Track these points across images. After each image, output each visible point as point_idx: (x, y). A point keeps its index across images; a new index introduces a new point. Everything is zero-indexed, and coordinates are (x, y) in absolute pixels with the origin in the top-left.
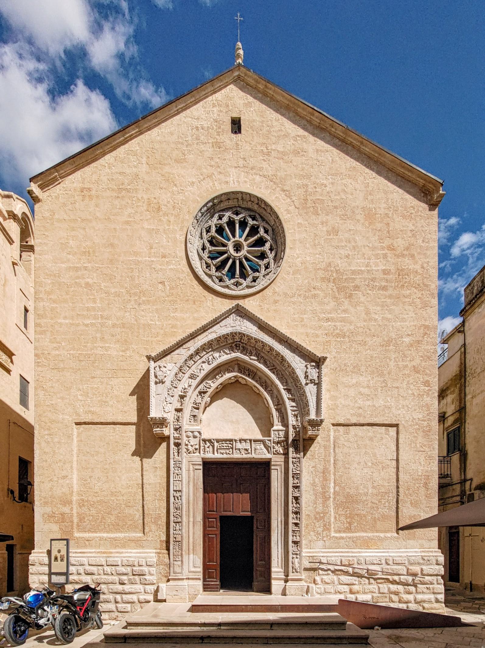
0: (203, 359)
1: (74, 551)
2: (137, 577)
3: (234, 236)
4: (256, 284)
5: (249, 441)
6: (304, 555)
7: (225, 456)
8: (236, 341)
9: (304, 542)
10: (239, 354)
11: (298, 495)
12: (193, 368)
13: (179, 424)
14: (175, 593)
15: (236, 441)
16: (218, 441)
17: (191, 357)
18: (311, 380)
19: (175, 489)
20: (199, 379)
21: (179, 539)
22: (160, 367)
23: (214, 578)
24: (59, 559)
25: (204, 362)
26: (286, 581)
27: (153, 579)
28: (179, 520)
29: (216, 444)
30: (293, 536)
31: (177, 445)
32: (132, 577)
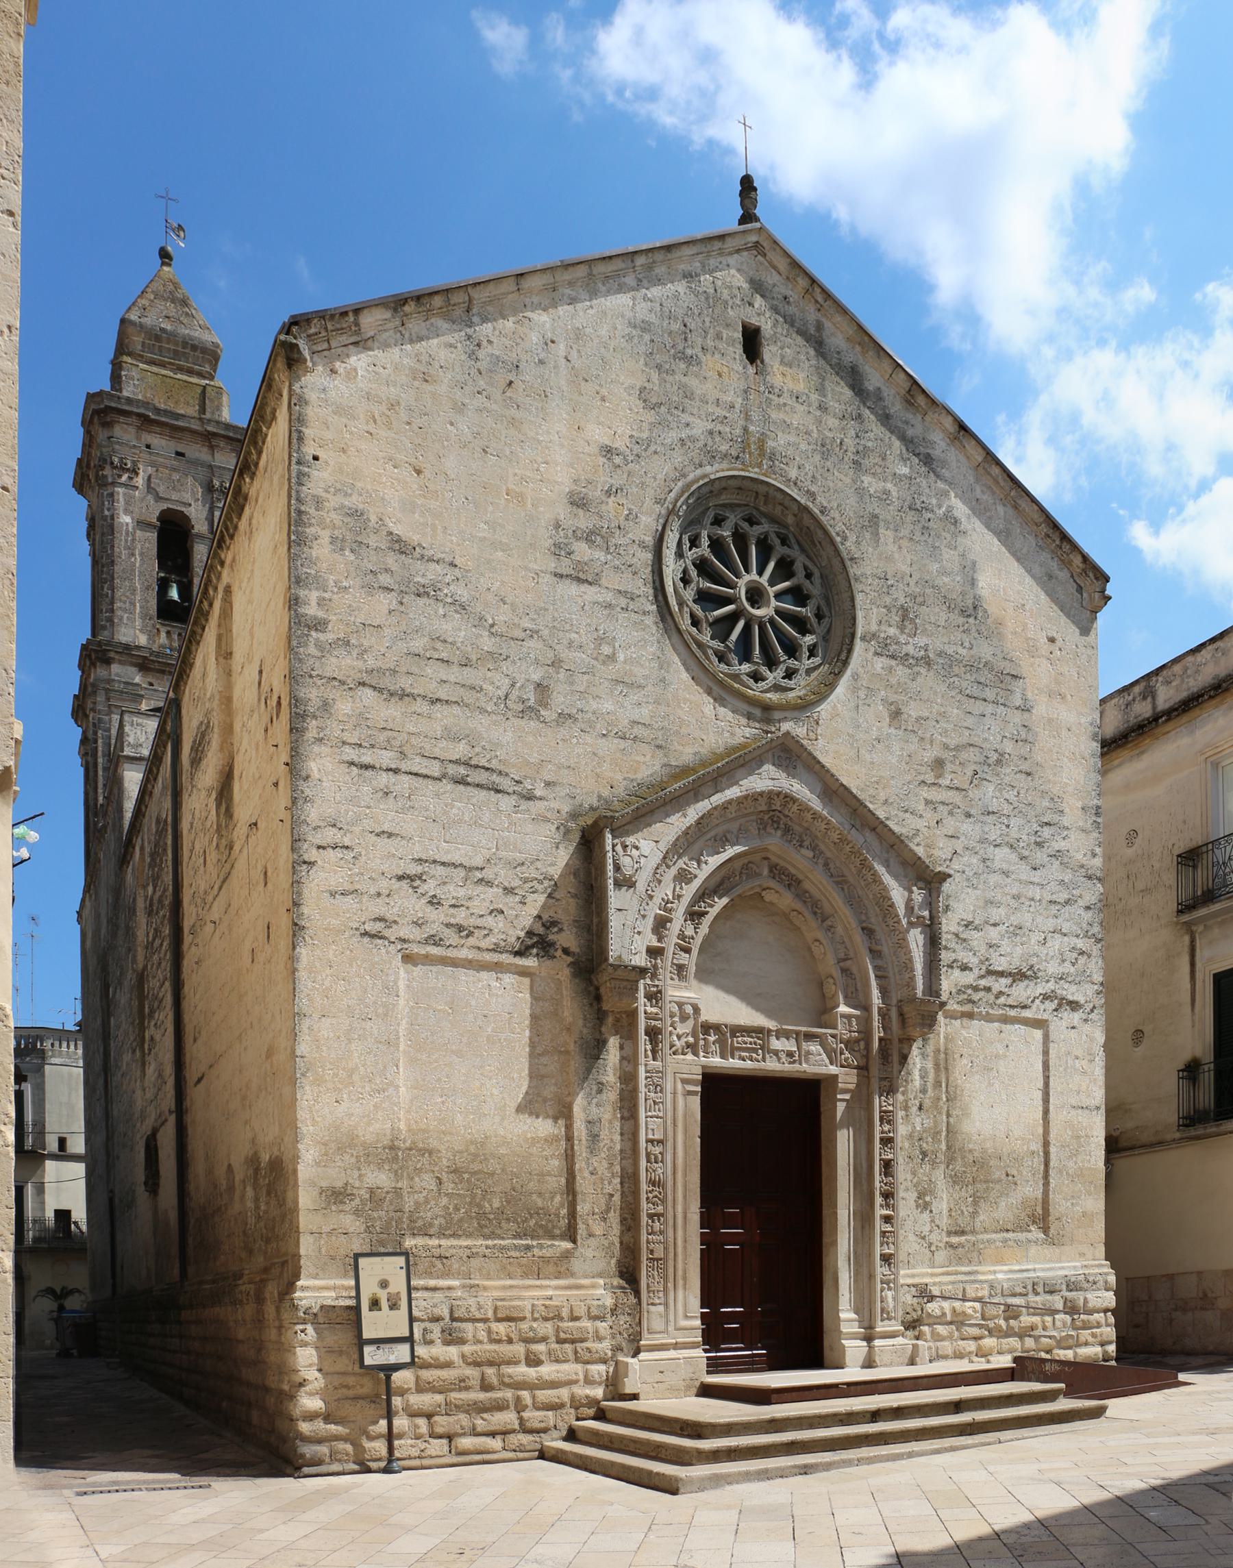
1: (422, 1283)
2: (568, 1347)
3: (747, 571)
4: (791, 683)
6: (902, 1281)
8: (773, 812)
9: (902, 1256)
11: (890, 1156)
13: (657, 983)
14: (659, 1377)
19: (651, 1136)
20: (696, 884)
21: (659, 1253)
22: (625, 847)
24: (384, 1304)
26: (869, 1339)
27: (605, 1347)
28: (660, 1209)
32: (555, 1346)
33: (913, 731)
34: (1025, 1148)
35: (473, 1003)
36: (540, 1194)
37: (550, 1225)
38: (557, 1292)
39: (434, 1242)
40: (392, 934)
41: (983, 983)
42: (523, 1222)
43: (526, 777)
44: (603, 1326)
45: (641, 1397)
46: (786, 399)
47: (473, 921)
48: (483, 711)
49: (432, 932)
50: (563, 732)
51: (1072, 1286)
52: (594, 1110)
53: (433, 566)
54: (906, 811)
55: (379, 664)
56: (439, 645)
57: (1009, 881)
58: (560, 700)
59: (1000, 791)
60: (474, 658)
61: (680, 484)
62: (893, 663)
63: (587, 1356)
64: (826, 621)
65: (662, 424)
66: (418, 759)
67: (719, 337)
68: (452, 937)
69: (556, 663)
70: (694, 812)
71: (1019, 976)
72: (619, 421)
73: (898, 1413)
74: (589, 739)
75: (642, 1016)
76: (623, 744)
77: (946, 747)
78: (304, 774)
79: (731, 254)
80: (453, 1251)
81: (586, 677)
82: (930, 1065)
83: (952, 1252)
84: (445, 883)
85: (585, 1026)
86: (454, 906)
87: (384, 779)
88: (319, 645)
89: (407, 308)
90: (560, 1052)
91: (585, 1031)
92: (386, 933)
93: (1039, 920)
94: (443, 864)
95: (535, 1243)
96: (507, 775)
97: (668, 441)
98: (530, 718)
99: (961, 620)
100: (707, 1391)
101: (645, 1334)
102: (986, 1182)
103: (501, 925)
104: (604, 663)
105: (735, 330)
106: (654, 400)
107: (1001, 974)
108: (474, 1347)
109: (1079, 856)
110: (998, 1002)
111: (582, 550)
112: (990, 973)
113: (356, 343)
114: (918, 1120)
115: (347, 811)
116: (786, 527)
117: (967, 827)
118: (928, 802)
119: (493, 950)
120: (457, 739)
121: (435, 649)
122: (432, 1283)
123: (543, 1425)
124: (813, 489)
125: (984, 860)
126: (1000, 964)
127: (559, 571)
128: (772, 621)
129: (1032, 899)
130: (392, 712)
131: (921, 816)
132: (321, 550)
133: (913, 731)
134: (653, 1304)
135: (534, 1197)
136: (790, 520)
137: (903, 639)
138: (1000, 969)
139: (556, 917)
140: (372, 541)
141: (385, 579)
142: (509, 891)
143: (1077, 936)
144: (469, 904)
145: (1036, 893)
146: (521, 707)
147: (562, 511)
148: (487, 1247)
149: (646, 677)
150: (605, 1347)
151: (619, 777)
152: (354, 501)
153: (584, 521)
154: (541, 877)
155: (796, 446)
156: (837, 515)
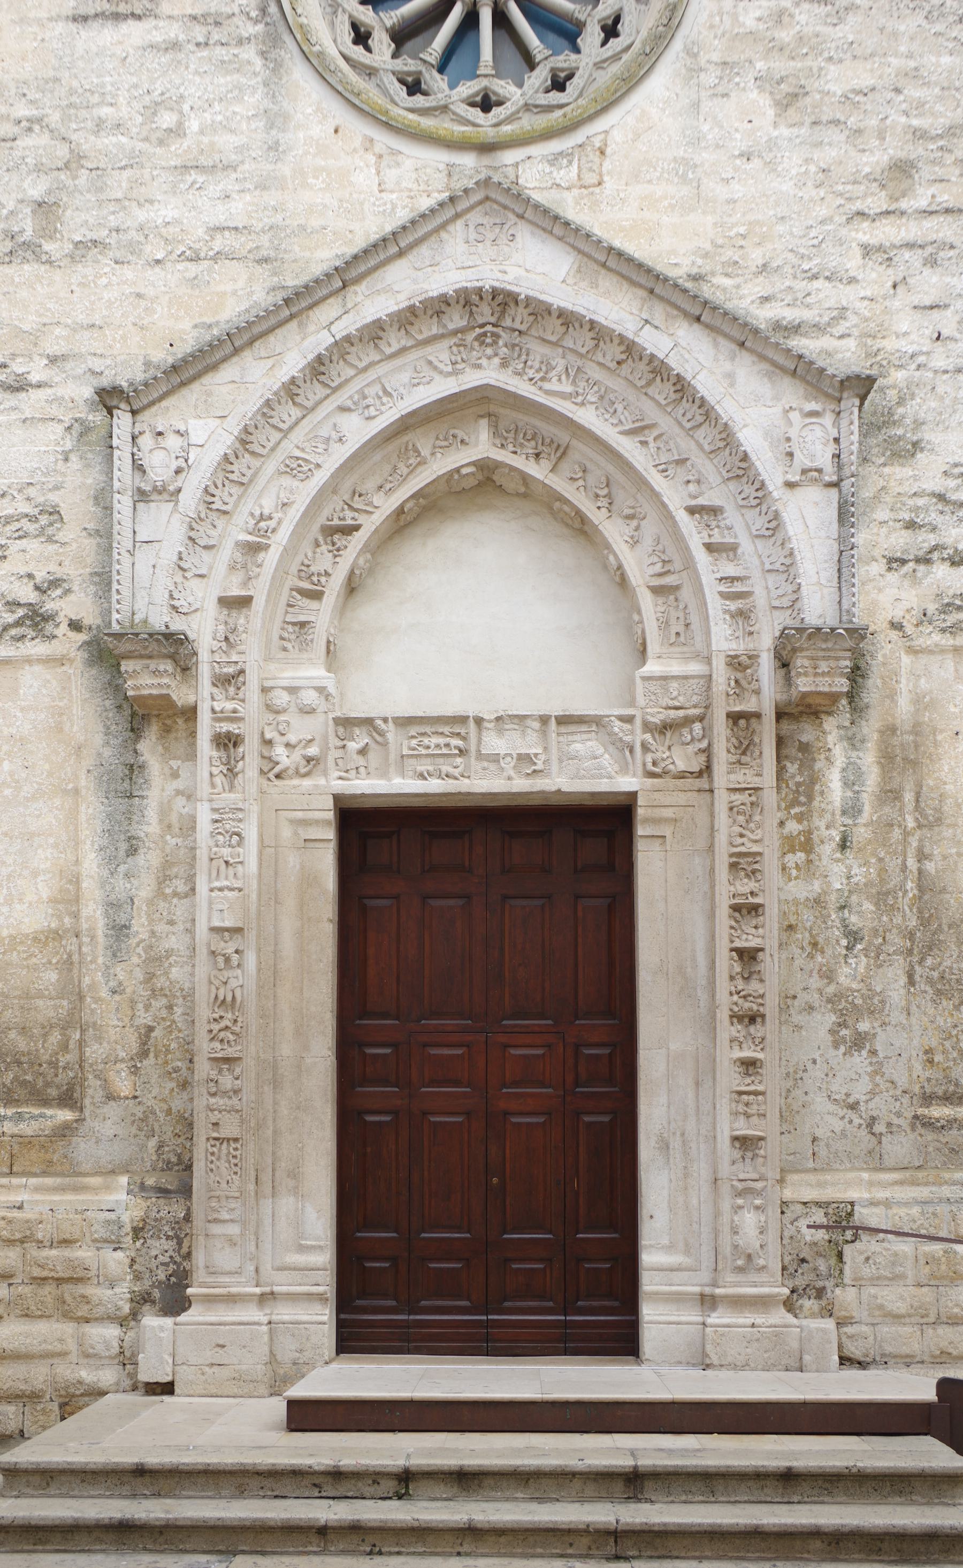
0: (342, 398)
2: (48, 1290)
5: (536, 725)
7: (434, 786)
8: (491, 313)
10: (494, 374)
11: (753, 943)
12: (298, 436)
13: (234, 658)
15: (479, 721)
16: (405, 722)
17: (291, 390)
18: (804, 472)
19: (217, 923)
20: (320, 478)
23: (385, 1296)
25: (343, 409)
29: (392, 733)
31: (227, 742)
33: (836, 122)
36: (23, 1030)
37: (40, 1083)
38: (38, 1197)
43: (14, 356)
44: (116, 1261)
50: (85, 270)
52: (121, 885)
54: (815, 277)
58: (78, 221)
63: (83, 1311)
70: (293, 352)
73: (466, 1480)
74: (128, 273)
77: (919, 135)
82: (869, 759)
83: (930, 1136)
90: (65, 792)
91: (107, 752)
98: (25, 260)
101: (200, 1275)
104: (161, 142)
114: (838, 870)
118: (867, 251)
131: (852, 280)
133: (836, 122)
134: (216, 1221)
149: (240, 149)
150: (119, 1296)
151: (186, 325)
154: (36, 511)
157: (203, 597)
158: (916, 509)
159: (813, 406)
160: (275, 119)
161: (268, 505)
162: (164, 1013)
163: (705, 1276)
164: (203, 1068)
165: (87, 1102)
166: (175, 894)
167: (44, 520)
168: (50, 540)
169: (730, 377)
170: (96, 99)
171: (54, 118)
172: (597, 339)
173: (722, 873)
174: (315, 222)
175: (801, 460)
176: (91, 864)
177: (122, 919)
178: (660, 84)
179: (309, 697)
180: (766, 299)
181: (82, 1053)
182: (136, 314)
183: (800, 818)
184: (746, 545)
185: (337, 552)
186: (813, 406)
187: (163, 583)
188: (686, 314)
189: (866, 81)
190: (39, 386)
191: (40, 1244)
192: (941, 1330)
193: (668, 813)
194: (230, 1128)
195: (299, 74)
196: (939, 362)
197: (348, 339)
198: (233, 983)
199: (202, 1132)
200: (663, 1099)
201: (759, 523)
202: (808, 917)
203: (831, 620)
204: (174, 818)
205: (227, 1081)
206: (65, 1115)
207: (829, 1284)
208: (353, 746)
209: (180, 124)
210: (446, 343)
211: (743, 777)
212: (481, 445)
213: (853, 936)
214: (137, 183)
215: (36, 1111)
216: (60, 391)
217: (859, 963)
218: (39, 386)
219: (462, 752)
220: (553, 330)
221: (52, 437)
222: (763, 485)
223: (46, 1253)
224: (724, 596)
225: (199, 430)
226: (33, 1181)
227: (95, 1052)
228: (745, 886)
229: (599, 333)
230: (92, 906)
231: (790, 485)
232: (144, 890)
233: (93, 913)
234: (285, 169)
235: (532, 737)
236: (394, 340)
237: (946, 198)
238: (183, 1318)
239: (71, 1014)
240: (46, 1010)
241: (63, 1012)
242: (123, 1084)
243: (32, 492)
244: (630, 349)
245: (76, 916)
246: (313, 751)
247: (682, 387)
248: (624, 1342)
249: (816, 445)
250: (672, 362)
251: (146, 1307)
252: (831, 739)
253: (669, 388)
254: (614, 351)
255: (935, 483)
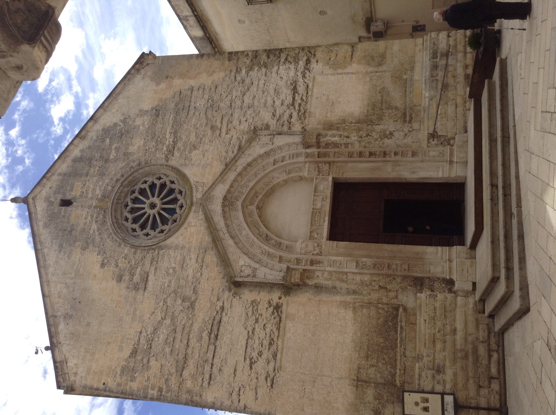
7: (327, 219)
8: (228, 202)
11: (368, 153)
12: (246, 244)
15: (313, 209)
17: (236, 243)
24: (426, 405)
30: (407, 156)
31: (312, 263)
33: (201, 140)
34: (368, 84)
35: (299, 341)
36: (378, 319)
37: (392, 316)
39: (398, 371)
40: (272, 374)
41: (297, 107)
42: (390, 328)
43: (216, 309)
44: (440, 297)
45: (474, 281)
46: (84, 190)
47: (268, 338)
48: (192, 325)
49: (272, 356)
51: (434, 55)
53: (141, 341)
55: (174, 367)
56: (168, 341)
57: (257, 96)
58: (188, 292)
59: (223, 100)
60: (173, 327)
61: (114, 236)
62: (176, 148)
64: (162, 176)
65: (93, 241)
66: (208, 354)
67: (64, 216)
68: (274, 347)
69: (175, 292)
71: (295, 90)
72: (93, 259)
74: (202, 281)
75: (306, 267)
76: (204, 267)
77: (206, 125)
78: (212, 404)
79: (36, 209)
80: (402, 364)
81: (181, 281)
82: (330, 133)
83: (413, 120)
84: (254, 349)
85: (309, 292)
86: (262, 346)
87: (215, 370)
88: (167, 392)
89: (55, 342)
92: (271, 376)
93: (273, 80)
94: (246, 348)
95: (399, 324)
96: (214, 317)
97: (99, 239)
99: (160, 117)
100: (474, 246)
101: (444, 276)
102: (382, 103)
103: (269, 326)
104: (176, 272)
105: (62, 210)
106: (85, 244)
107: (294, 98)
108: (447, 360)
109: (248, 62)
110: (305, 100)
111: (137, 278)
112: (293, 104)
113: (66, 363)
115: (226, 388)
116: (128, 191)
117: (236, 115)
118: (227, 134)
119: (279, 330)
120: (201, 338)
121: (170, 343)
122: (417, 376)
123: (486, 331)
124: (115, 179)
125: (249, 108)
126: (289, 99)
127: (143, 288)
128: (162, 199)
129: (264, 84)
130: (191, 364)
131: (232, 136)
132: (134, 386)
133: (201, 140)
134: (429, 271)
135: (379, 322)
136: (126, 189)
137: (167, 143)
138: (291, 99)
139: (267, 301)
140: (132, 364)
141: (145, 361)
142: (257, 321)
143: (279, 61)
144: (261, 338)
145: (262, 82)
146: (191, 309)
147: (123, 285)
148: (401, 347)
149: (181, 255)
150: (450, 296)
151: (216, 269)
152: (119, 370)
153: (126, 277)
155: (101, 186)
156: (124, 170)
157: (278, 266)
158: (279, 125)
159: (258, 140)
160: (176, 248)
161: (258, 251)
162: (376, 282)
163: (445, 164)
164: (390, 272)
165: (397, 303)
166: (347, 278)
167: (254, 304)
168: (259, 303)
169: (249, 155)
170: (163, 287)
171: (165, 296)
172: (237, 181)
173: (352, 159)
174: (200, 240)
175: (268, 142)
176: (338, 298)
177: (351, 291)
178: (187, 171)
179: (304, 245)
180: (233, 152)
181: (385, 304)
182: (212, 279)
183: (341, 145)
184: (283, 154)
185: (271, 239)
186: (258, 140)
187: (274, 273)
188: (235, 163)
189: (194, 134)
190: (223, 303)
191: (435, 316)
192: (458, 116)
193: (338, 171)
194: (406, 267)
195: (168, 242)
196: (251, 121)
197: (227, 230)
198: (370, 264)
199: (406, 273)
200: (402, 173)
201: (279, 151)
202: (363, 144)
203: (301, 136)
204: (328, 277)
205: (394, 267)
206: (401, 310)
207: (447, 138)
208: (316, 236)
209: (173, 268)
210: (231, 213)
211: (332, 155)
212: (253, 208)
213: (368, 135)
214: (183, 279)
215: (400, 317)
216: (226, 298)
217: (374, 134)
218: (223, 303)
219: (320, 213)
220: (232, 190)
221: (236, 301)
222: (272, 149)
223: (438, 314)
224: (293, 159)
225: (241, 263)
226: (418, 318)
227: (385, 300)
228: (355, 155)
229: (235, 180)
230: (348, 298)
231: (273, 144)
232: (344, 286)
233: (349, 298)
234: (187, 246)
235: (318, 198)
236: (229, 222)
237: (219, 120)
238: (455, 280)
239: (374, 307)
240: (373, 312)
241: (374, 308)
242: (392, 294)
243: (247, 307)
244: (240, 174)
245: (350, 303)
246: (316, 245)
247: (249, 165)
248: (459, 187)
249: (265, 139)
250: (244, 165)
251: (453, 290)
252: (325, 140)
253: (249, 168)
254: (239, 179)
255: (275, 122)
